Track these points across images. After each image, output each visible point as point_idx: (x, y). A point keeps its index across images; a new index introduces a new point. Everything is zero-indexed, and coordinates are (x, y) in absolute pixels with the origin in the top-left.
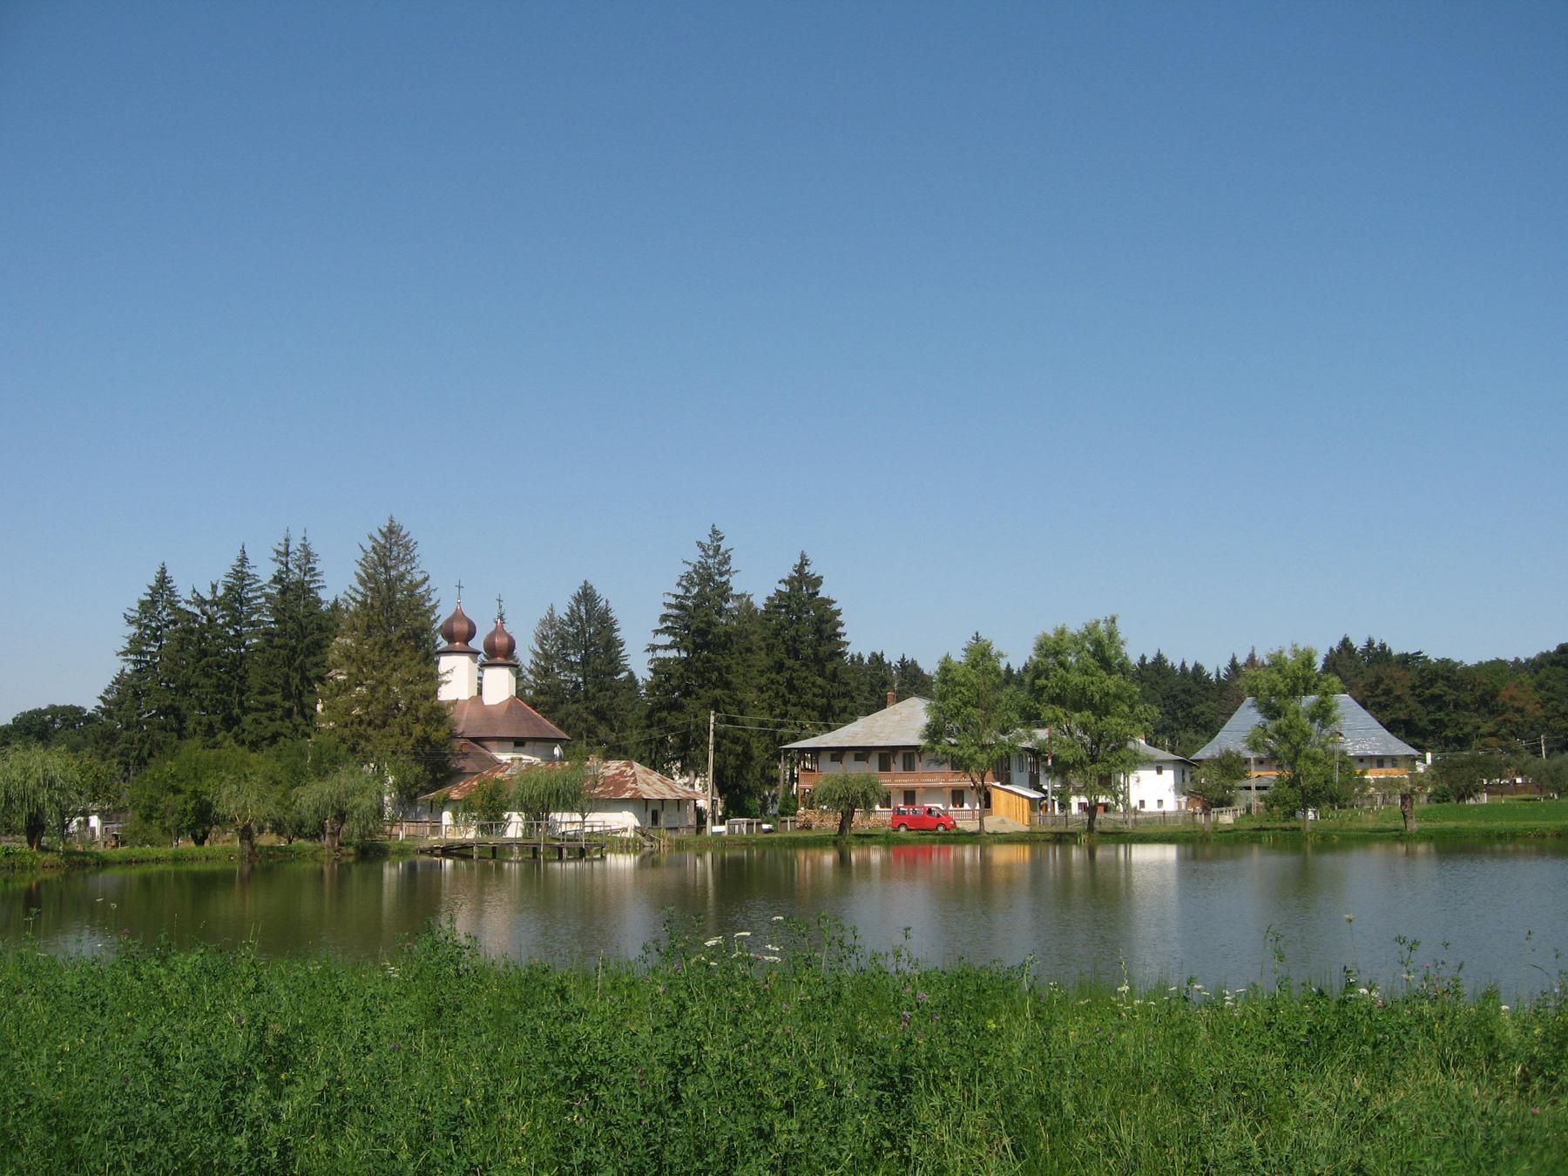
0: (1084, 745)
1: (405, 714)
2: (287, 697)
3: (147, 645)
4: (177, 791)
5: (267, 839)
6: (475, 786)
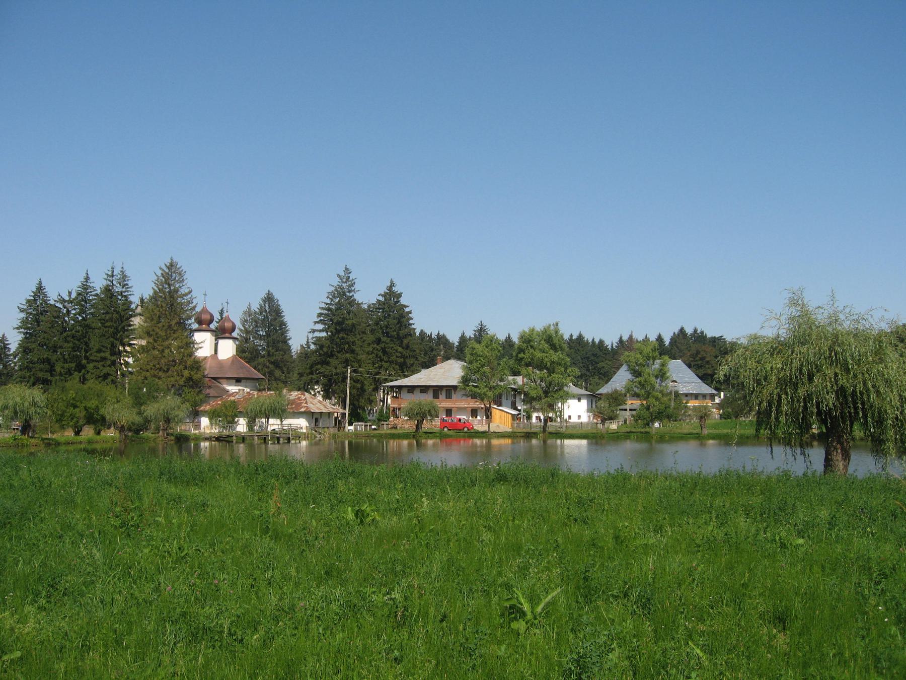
6: (219, 404)
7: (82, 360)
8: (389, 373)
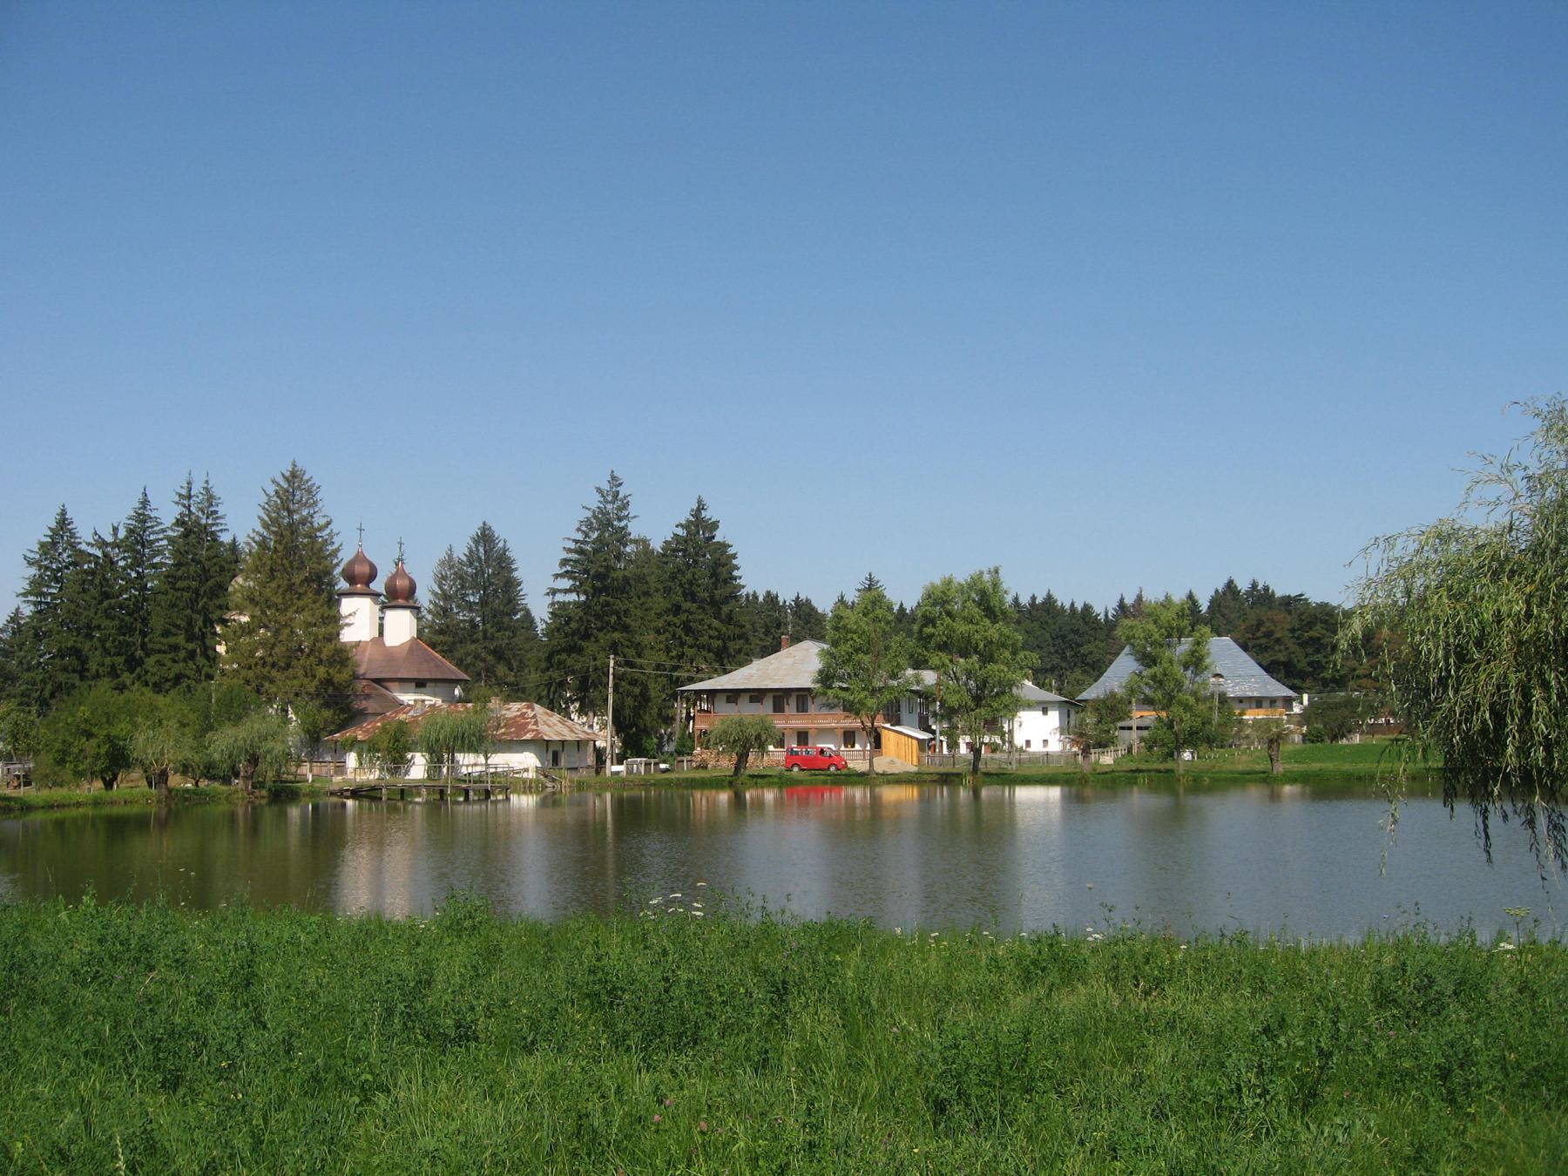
0: (969, 690)
1: (308, 656)
2: (190, 638)
3: (47, 586)
6: (378, 728)
7: (136, 650)
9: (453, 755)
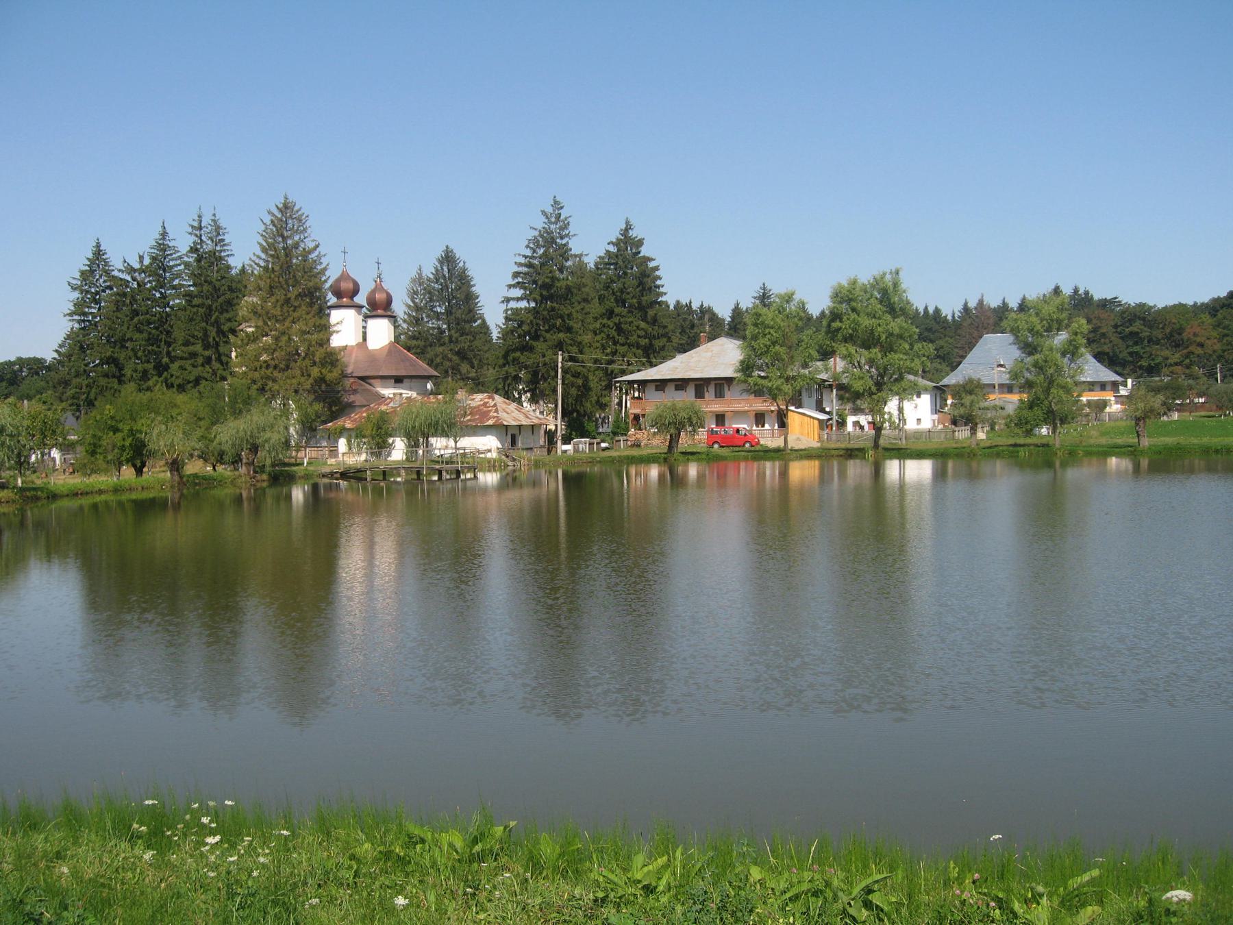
0: (871, 377)
1: (304, 358)
2: (206, 347)
3: (88, 307)
4: (116, 430)
5: (194, 467)
6: (364, 417)
7: (163, 358)
8: (628, 361)
9: (427, 439)
